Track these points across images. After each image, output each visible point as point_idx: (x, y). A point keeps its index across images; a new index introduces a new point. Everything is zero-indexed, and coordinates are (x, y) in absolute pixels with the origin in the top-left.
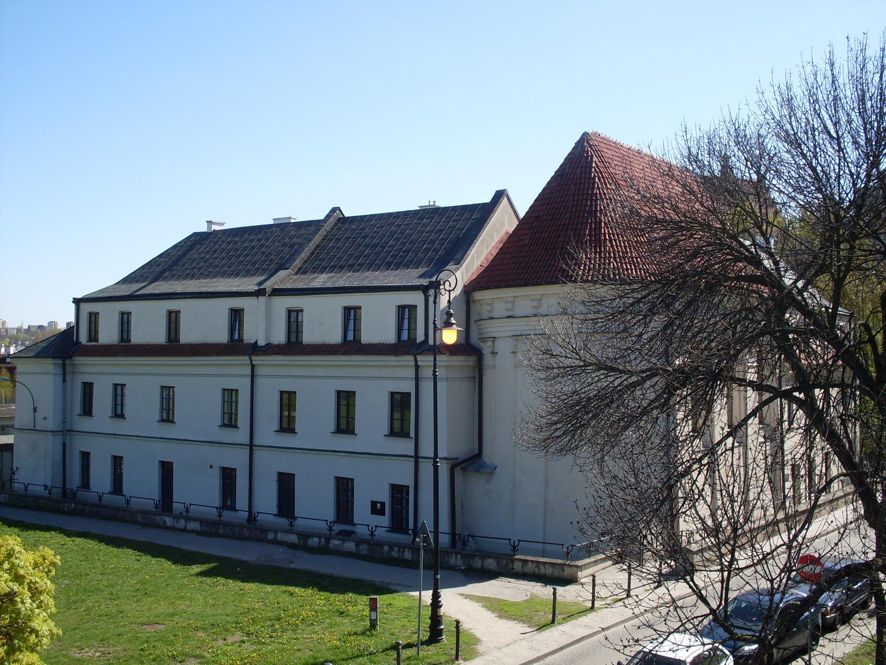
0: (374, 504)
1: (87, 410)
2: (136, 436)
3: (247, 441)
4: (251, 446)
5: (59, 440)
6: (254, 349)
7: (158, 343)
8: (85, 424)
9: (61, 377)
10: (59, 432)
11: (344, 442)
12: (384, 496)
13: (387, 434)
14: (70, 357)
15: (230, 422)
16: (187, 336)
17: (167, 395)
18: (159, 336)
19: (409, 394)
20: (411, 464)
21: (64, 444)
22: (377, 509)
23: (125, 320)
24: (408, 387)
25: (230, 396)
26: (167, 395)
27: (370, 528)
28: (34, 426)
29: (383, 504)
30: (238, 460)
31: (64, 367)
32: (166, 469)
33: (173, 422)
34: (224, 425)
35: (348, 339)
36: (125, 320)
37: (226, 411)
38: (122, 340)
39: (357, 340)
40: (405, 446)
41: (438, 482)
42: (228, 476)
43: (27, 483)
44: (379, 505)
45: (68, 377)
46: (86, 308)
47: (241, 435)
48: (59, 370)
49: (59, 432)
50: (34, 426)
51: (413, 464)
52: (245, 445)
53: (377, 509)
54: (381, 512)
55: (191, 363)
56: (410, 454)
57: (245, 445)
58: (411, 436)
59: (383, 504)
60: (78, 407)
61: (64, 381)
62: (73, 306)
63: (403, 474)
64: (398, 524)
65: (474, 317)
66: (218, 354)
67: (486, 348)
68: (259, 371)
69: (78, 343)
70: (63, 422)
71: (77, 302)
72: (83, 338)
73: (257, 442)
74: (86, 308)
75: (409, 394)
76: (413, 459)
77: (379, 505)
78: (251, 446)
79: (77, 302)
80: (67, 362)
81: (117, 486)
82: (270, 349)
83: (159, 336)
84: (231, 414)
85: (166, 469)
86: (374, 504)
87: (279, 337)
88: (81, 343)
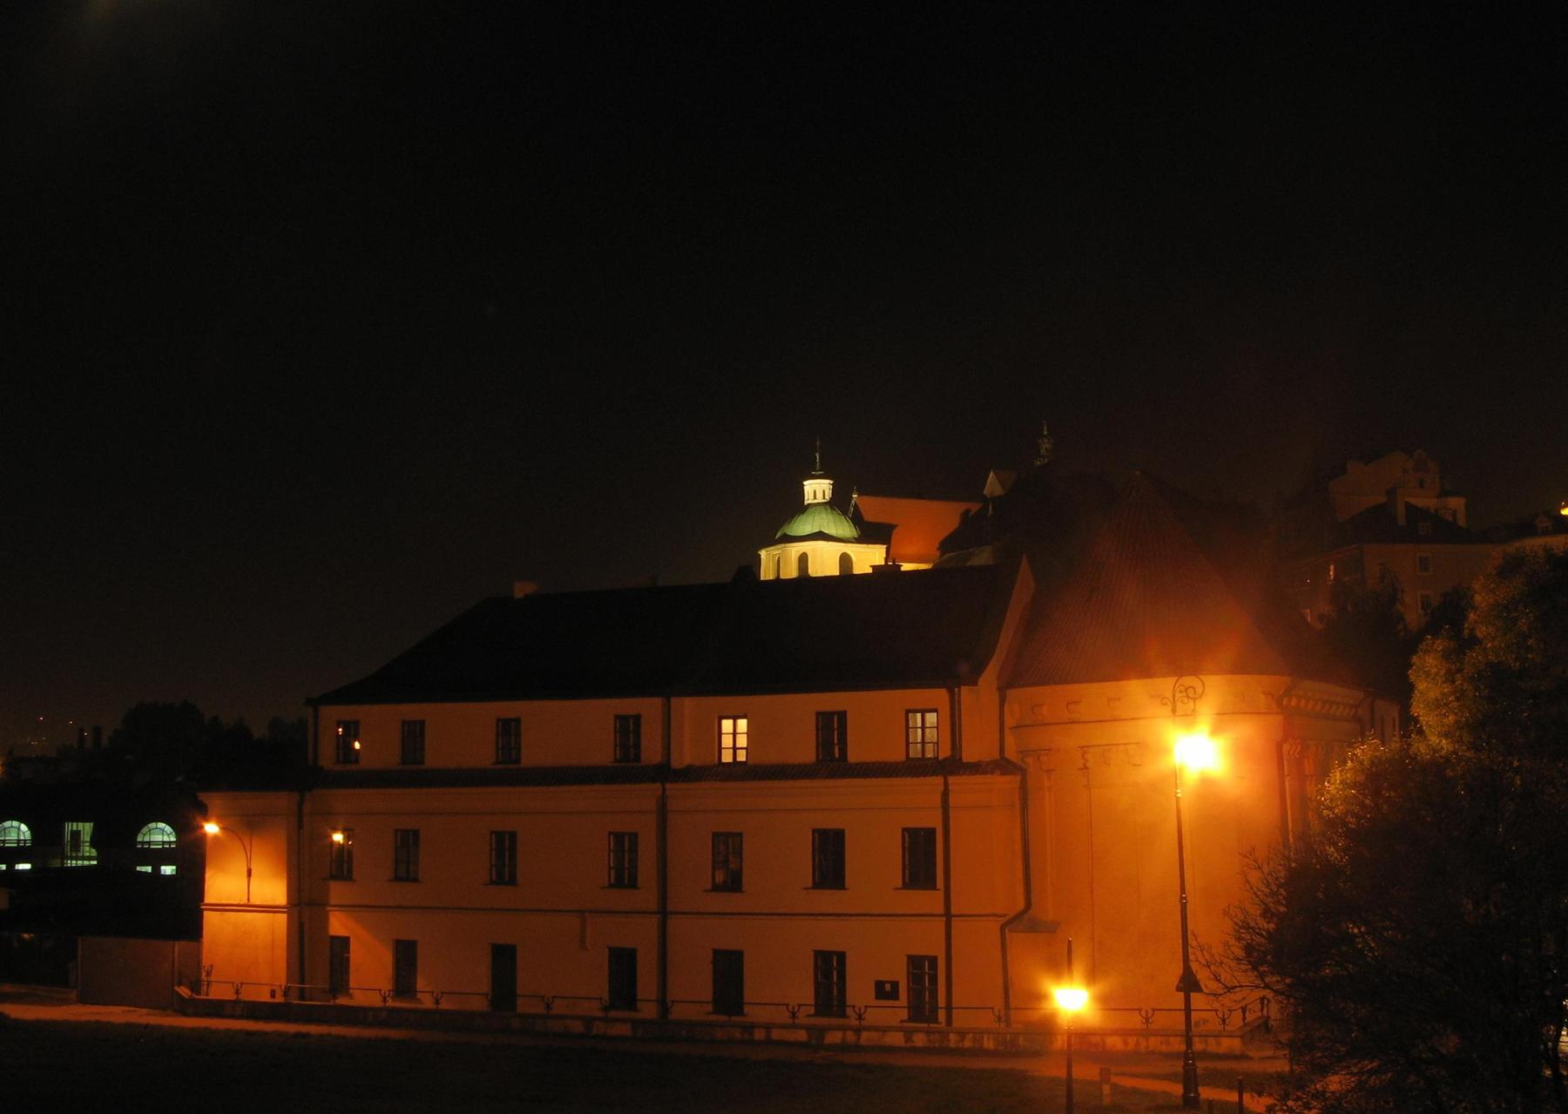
0: (879, 985)
3: (941, 911)
4: (948, 915)
12: (899, 973)
15: (624, 878)
17: (505, 847)
18: (483, 755)
19: (932, 832)
22: (885, 991)
24: (933, 821)
25: (624, 844)
26: (505, 847)
27: (857, 1010)
28: (248, 900)
29: (895, 985)
30: (640, 935)
32: (504, 957)
34: (492, 882)
40: (929, 901)
42: (623, 963)
44: (888, 987)
47: (646, 896)
52: (749, 1003)
53: (885, 991)
54: (894, 994)
56: (936, 912)
57: (749, 1003)
58: (938, 888)
61: (300, 827)
63: (928, 941)
64: (922, 1010)
73: (954, 911)
75: (932, 832)
76: (944, 919)
77: (888, 987)
78: (948, 915)
83: (483, 755)
85: (504, 957)
86: (879, 985)
87: (805, 752)
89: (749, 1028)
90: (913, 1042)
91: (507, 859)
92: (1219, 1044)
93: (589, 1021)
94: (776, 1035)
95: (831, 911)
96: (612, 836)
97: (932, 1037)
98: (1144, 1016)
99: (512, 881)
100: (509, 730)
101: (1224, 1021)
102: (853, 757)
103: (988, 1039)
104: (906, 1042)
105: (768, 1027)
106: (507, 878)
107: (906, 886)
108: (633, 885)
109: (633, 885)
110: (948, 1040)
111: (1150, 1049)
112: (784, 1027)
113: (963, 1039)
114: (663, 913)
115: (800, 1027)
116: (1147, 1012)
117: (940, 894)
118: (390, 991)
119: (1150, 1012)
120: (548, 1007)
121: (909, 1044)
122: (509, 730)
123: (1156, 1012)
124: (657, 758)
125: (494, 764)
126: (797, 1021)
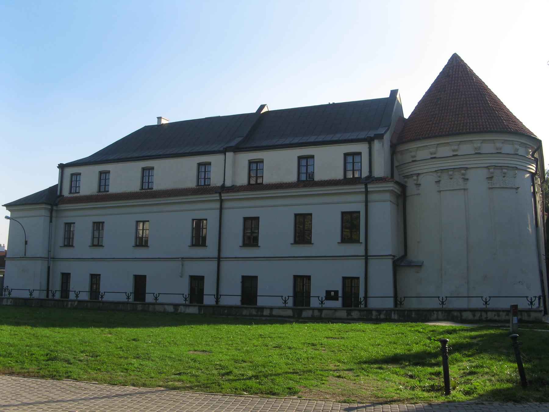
0: (328, 293)
1: (69, 243)
2: (92, 259)
4: (366, 257)
5: (45, 264)
6: (223, 189)
7: (133, 191)
8: (67, 253)
9: (48, 219)
10: (46, 258)
11: (303, 250)
12: (338, 287)
13: (241, 245)
14: (56, 205)
16: (268, 178)
18: (135, 186)
20: (362, 262)
21: (49, 268)
23: (104, 176)
24: (361, 208)
26: (98, 226)
28: (25, 255)
29: (336, 292)
31: (51, 211)
33: (72, 246)
34: (136, 246)
35: (355, 177)
36: (104, 176)
37: (66, 237)
38: (99, 191)
39: (311, 176)
40: (357, 249)
41: (95, 274)
43: (156, 292)
44: (333, 293)
45: (54, 219)
46: (69, 171)
47: (210, 250)
48: (48, 214)
49: (46, 258)
50: (25, 255)
51: (216, 262)
53: (330, 296)
54: (336, 298)
55: (169, 202)
58: (360, 242)
59: (336, 292)
60: (60, 241)
61: (51, 221)
62: (57, 171)
65: (396, 164)
66: (192, 194)
67: (410, 184)
68: (371, 197)
69: (61, 195)
70: (49, 251)
71: (62, 167)
72: (66, 193)
73: (369, 254)
74: (69, 171)
77: (333, 293)
78: (366, 257)
79: (62, 167)
80: (55, 208)
81: (218, 297)
82: (233, 189)
84: (69, 238)
86: (328, 293)
87: (242, 180)
88: (64, 196)
89: (262, 309)
90: (352, 316)
91: (308, 232)
92: (529, 316)
93: (176, 306)
94: (275, 312)
95: (109, 258)
96: (67, 226)
97: (362, 313)
98: (185, 297)
99: (308, 242)
100: (147, 172)
101: (285, 301)
102: (317, 178)
103: (394, 314)
104: (348, 316)
105: (271, 309)
106: (144, 244)
107: (193, 245)
108: (204, 244)
109: (204, 244)
110: (372, 315)
111: (489, 318)
112: (280, 308)
113: (380, 315)
114: (219, 259)
115: (289, 308)
116: (322, 298)
117: (363, 246)
118: (131, 293)
119: (78, 293)
120: (156, 299)
121: (349, 317)
122: (147, 172)
123: (80, 292)
124: (220, 184)
125: (97, 192)
126: (287, 305)
